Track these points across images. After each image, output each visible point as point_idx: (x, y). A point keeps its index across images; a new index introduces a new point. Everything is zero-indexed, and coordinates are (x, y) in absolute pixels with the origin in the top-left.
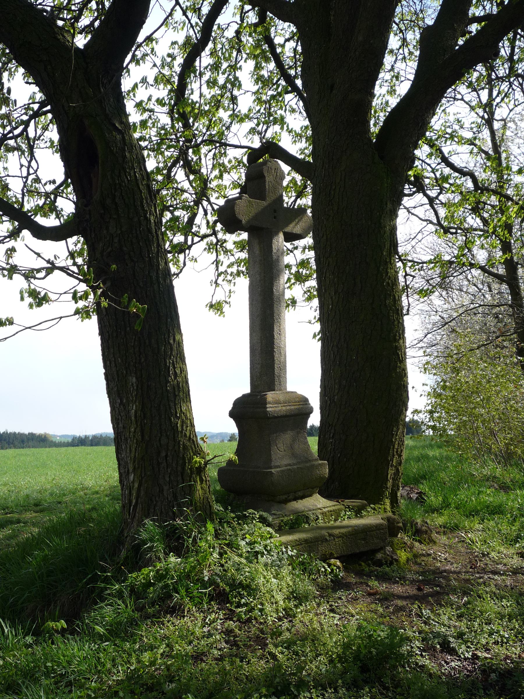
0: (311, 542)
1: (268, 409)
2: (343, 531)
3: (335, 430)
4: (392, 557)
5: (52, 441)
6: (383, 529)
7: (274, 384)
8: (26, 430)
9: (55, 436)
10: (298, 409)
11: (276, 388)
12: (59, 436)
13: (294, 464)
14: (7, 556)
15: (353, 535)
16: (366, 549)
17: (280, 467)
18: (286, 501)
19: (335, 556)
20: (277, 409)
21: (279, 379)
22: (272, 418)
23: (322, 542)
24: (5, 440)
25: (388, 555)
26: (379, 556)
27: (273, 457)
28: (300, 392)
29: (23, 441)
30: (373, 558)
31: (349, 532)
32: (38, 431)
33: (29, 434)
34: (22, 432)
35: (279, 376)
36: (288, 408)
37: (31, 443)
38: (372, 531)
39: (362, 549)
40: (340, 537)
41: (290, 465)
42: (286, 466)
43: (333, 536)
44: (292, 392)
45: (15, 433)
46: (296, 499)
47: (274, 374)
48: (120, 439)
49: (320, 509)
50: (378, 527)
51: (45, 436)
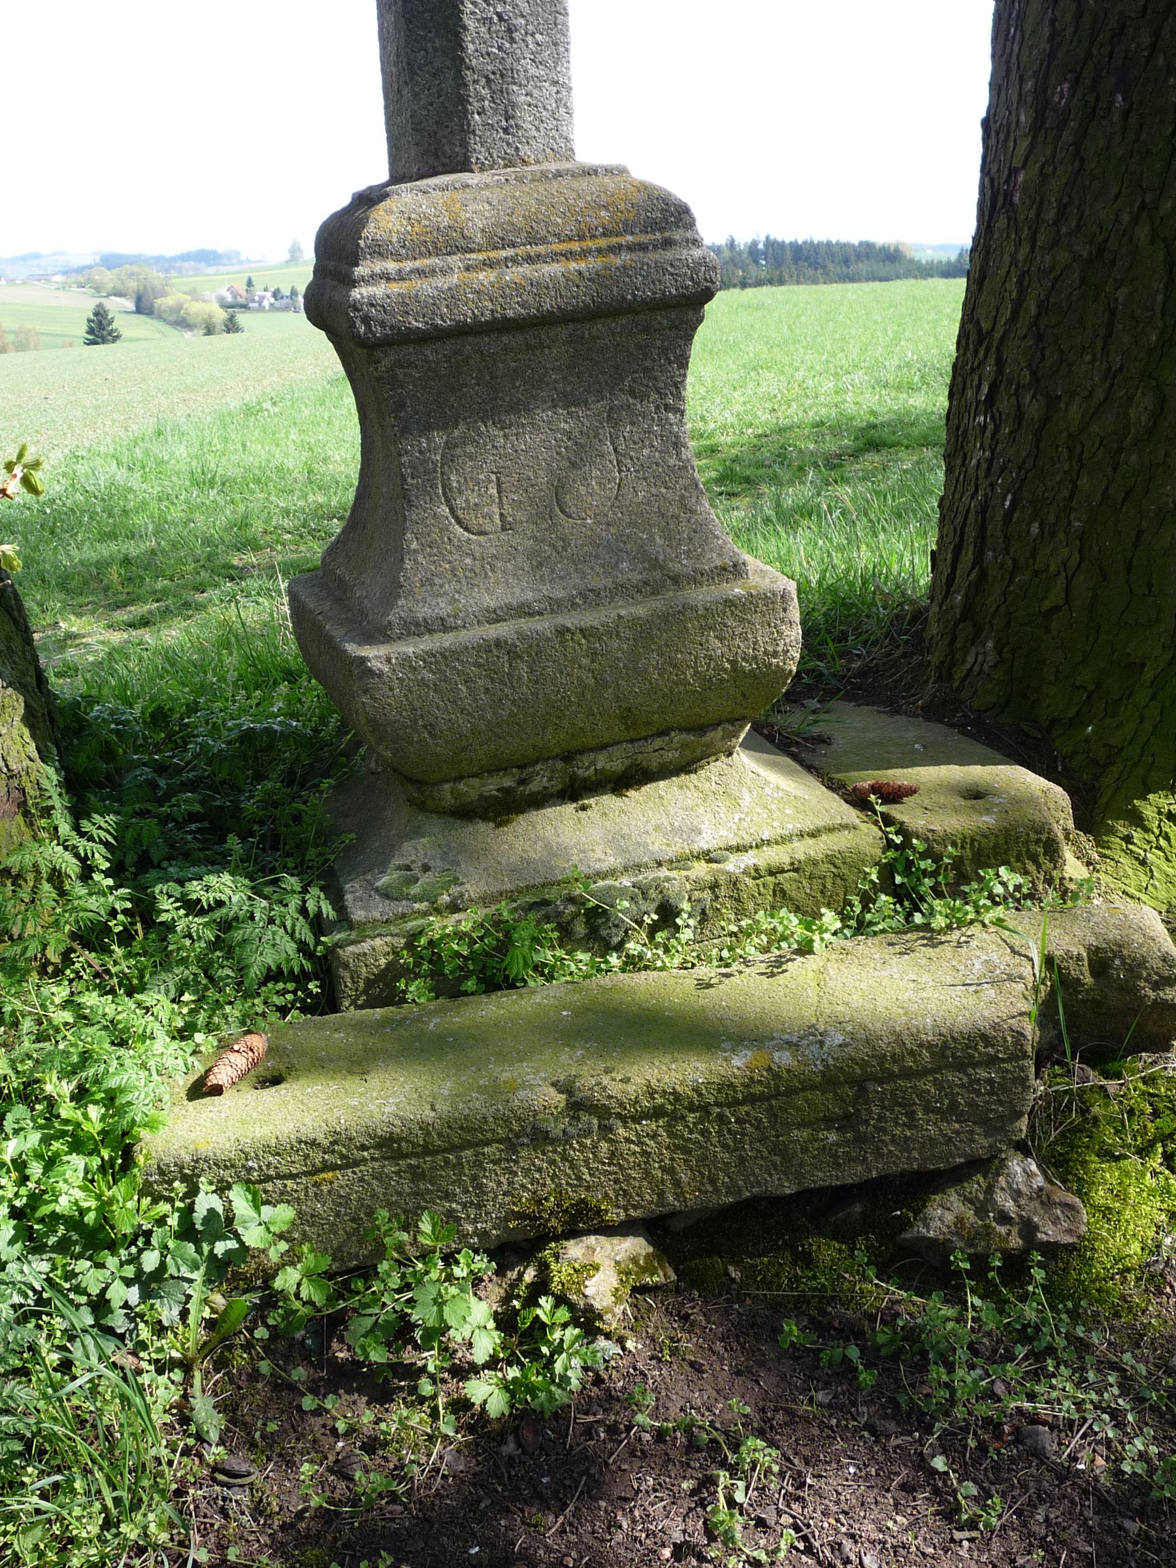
0: (427, 1150)
1: (359, 293)
2: (686, 1072)
3: (1000, 364)
4: (1028, 1229)
5: (912, 261)
6: (991, 1061)
7: (466, 130)
8: (852, 235)
9: (923, 248)
10: (596, 278)
11: (479, 153)
12: (933, 248)
13: (555, 606)
14: (425, 620)
15: (751, 1099)
16: (853, 1174)
17: (445, 628)
18: (504, 809)
19: (615, 1215)
20: (426, 287)
21: (499, 94)
22: (387, 343)
23: (512, 1146)
24: (807, 259)
25: (1004, 1218)
26: (943, 1215)
27: (418, 562)
28: (642, 172)
29: (846, 261)
30: (906, 1224)
31: (726, 1086)
32: (881, 237)
33: (861, 243)
34: (843, 240)
35: (501, 79)
36: (514, 274)
37: (863, 267)
38: (907, 1074)
39: (822, 1177)
40: (656, 1113)
41: (524, 611)
42: (495, 617)
43: (601, 1112)
44: (609, 171)
45: (829, 244)
46: (575, 791)
47: (458, 63)
48: (984, 265)
49: (708, 857)
50: (960, 1054)
51: (897, 250)
